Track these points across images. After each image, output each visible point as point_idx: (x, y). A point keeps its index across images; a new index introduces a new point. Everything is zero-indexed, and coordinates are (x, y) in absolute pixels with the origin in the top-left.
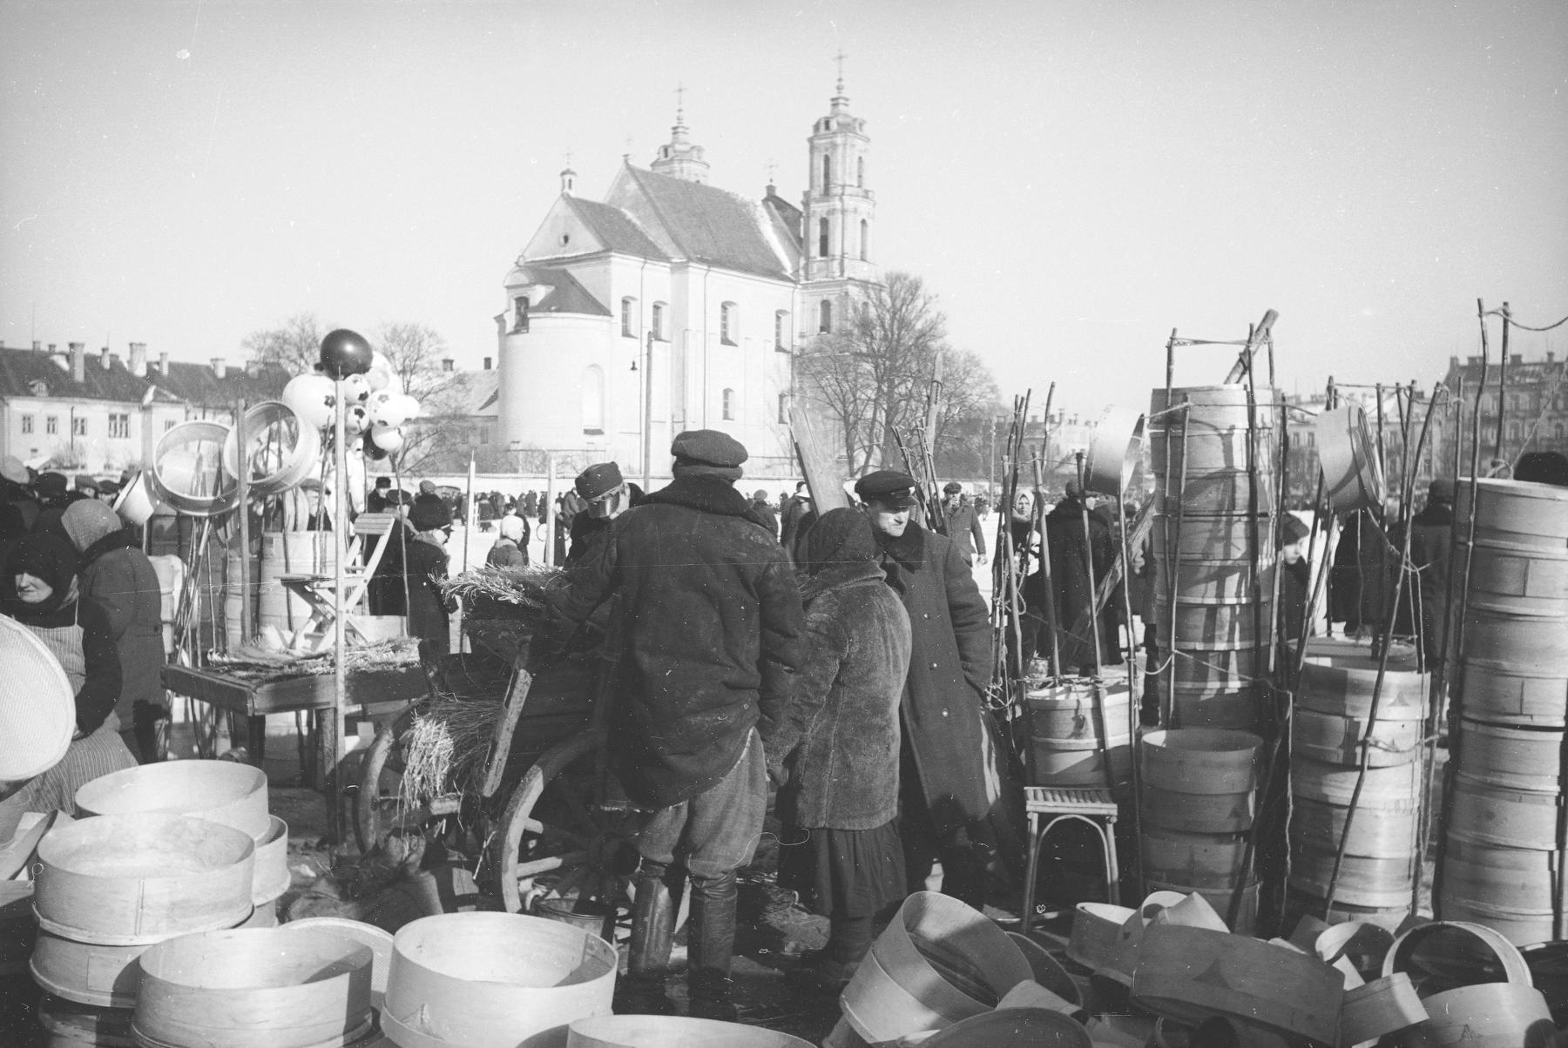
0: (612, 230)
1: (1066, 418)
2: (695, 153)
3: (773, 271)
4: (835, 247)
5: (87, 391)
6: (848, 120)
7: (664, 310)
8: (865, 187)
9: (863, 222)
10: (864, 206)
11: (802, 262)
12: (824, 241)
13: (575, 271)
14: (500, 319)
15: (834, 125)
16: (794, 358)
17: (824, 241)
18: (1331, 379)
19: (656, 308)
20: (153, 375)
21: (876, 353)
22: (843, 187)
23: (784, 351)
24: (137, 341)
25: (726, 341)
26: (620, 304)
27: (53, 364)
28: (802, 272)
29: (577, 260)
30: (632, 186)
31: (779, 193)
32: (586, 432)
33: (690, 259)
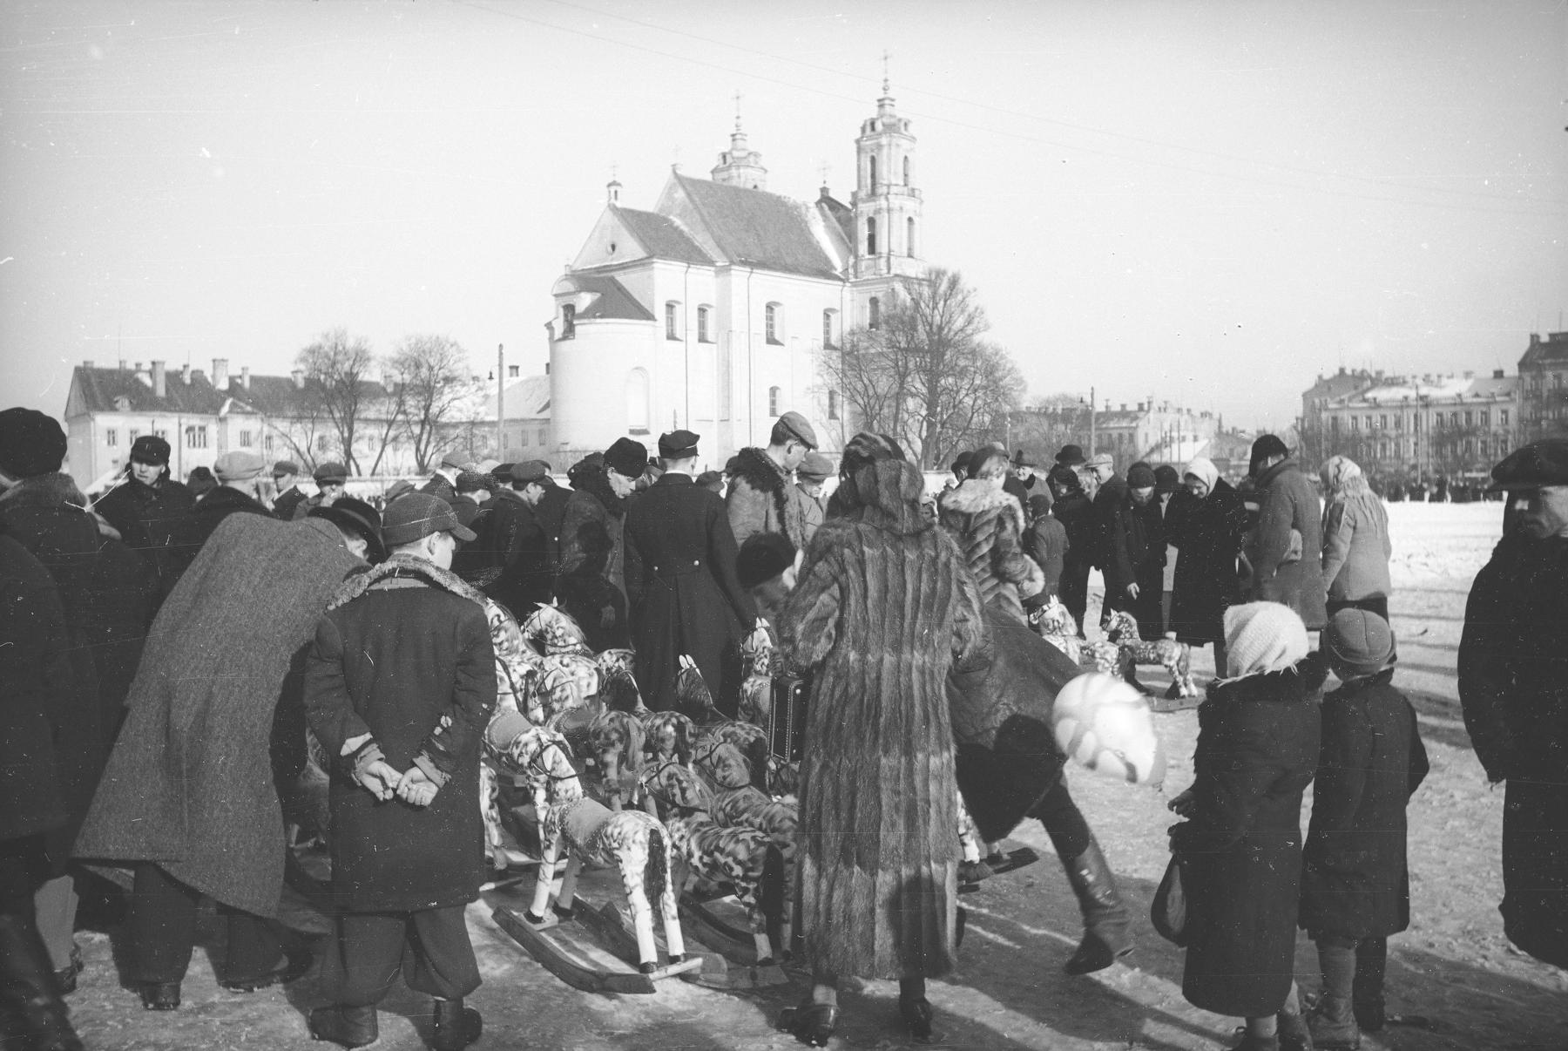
0: (658, 236)
1: (1155, 406)
2: (752, 158)
3: (823, 271)
4: (882, 246)
6: (893, 120)
7: (710, 314)
9: (910, 219)
10: (910, 205)
11: (852, 260)
12: (872, 240)
13: (621, 277)
14: (549, 326)
15: (879, 127)
17: (872, 240)
19: (702, 311)
20: (234, 389)
21: (915, 343)
22: (889, 186)
23: (835, 348)
24: (219, 357)
25: (771, 340)
26: (696, 312)
28: (851, 271)
29: (623, 267)
30: (680, 194)
31: (832, 195)
33: (732, 263)
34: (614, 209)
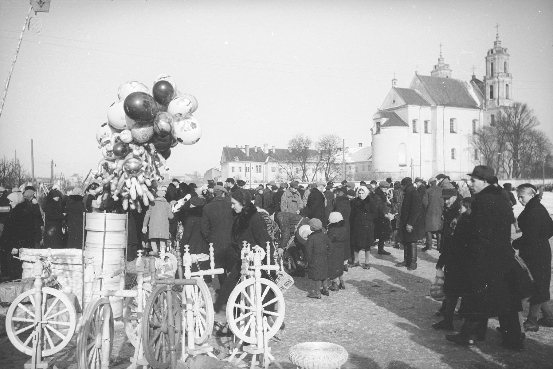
0: (410, 97)
3: (473, 106)
4: (496, 95)
5: (249, 159)
6: (500, 49)
8: (507, 72)
9: (507, 85)
10: (507, 80)
13: (396, 112)
14: (372, 130)
15: (494, 52)
16: (481, 136)
18: (468, 174)
22: (498, 73)
25: (452, 131)
27: (241, 151)
28: (483, 105)
29: (397, 108)
31: (477, 78)
32: (400, 166)
33: (437, 105)
34: (394, 88)
